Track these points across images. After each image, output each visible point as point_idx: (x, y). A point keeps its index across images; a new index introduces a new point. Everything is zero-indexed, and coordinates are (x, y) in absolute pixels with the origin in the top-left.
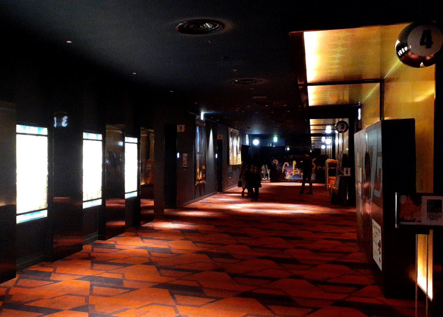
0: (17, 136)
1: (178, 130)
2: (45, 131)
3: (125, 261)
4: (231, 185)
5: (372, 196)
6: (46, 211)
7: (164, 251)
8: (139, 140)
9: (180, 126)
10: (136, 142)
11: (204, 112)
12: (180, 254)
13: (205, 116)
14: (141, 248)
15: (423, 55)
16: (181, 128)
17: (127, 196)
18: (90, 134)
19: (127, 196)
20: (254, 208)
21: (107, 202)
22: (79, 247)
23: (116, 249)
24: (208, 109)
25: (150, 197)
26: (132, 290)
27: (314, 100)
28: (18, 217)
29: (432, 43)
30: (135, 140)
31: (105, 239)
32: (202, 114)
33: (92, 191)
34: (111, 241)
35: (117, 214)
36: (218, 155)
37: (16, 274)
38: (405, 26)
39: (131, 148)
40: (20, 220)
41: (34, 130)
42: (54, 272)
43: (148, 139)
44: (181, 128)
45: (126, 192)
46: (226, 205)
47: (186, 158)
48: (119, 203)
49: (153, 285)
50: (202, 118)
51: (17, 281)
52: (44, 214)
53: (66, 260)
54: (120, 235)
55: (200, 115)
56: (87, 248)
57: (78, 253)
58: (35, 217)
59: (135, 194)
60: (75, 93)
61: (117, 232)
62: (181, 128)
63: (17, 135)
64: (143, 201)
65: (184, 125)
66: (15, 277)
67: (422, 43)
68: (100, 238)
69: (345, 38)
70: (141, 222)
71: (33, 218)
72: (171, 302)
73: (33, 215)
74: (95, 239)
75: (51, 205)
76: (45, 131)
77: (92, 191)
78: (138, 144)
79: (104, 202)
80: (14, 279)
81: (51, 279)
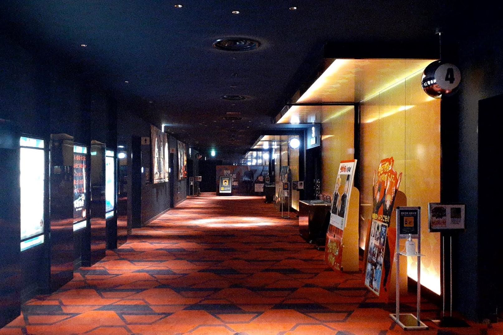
5: (440, 206)
7: (168, 272)
9: (144, 138)
10: (113, 155)
12: (186, 274)
14: (139, 271)
15: (444, 88)
21: (52, 223)
24: (167, 121)
26: (167, 314)
29: (454, 80)
34: (98, 266)
38: (428, 63)
44: (146, 140)
48: (60, 225)
49: (185, 307)
52: (41, 240)
54: (102, 260)
56: (77, 275)
57: (70, 283)
60: (86, 101)
61: (100, 256)
62: (146, 140)
63: (21, 149)
66: (19, 315)
67: (447, 79)
68: (84, 265)
69: (356, 67)
72: (217, 322)
74: (79, 266)
78: (46, 149)
79: (89, 224)
80: (19, 317)
81: (65, 311)
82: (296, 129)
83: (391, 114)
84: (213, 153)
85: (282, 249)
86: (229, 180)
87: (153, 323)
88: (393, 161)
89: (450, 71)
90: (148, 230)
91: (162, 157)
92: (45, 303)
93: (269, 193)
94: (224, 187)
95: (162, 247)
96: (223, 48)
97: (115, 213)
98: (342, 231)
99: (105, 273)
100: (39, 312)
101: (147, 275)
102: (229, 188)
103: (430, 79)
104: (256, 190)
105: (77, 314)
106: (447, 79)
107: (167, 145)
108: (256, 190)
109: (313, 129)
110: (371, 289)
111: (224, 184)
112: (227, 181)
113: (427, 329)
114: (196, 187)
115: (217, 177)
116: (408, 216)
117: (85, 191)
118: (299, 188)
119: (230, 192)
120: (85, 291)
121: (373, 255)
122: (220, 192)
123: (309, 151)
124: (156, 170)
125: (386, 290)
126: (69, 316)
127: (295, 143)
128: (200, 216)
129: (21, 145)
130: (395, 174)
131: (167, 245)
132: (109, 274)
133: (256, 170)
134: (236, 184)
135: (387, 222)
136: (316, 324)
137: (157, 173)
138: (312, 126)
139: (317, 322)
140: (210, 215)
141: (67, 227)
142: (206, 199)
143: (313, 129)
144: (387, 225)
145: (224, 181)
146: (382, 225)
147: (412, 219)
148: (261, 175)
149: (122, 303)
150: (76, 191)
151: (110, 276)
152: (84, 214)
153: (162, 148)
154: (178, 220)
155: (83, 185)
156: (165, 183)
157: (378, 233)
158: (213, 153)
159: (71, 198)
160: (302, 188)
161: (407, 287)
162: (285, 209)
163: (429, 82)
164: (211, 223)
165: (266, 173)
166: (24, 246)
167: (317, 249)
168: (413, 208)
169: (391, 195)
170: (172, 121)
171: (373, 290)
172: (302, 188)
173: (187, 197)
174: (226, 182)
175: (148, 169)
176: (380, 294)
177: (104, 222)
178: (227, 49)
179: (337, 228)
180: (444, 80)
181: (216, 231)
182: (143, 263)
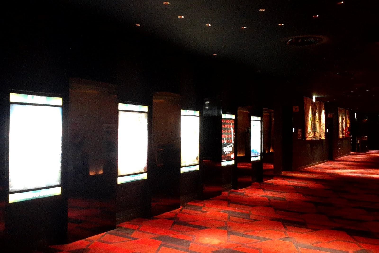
0: (182, 116)
1: (294, 110)
2: (198, 113)
3: (253, 203)
4: (341, 155)
6: (59, 189)
7: (284, 199)
8: (261, 119)
11: (315, 95)
13: (317, 99)
16: (295, 109)
17: (253, 159)
18: (226, 115)
19: (253, 159)
20: (357, 173)
21: (238, 164)
22: (220, 193)
23: (244, 195)
25: (271, 162)
27: (324, 136)
28: (119, 179)
30: (259, 118)
31: (237, 189)
32: (314, 98)
33: (190, 156)
35: (244, 172)
36: (328, 130)
37: (180, 206)
39: (256, 125)
40: (120, 181)
41: (191, 112)
42: (204, 206)
43: (270, 117)
45: (11, 189)
46: (335, 170)
47: (300, 132)
50: (314, 100)
51: (181, 210)
52: (144, 176)
53: (210, 200)
55: (312, 98)
58: (135, 179)
59: (259, 158)
62: (296, 109)
64: (264, 165)
65: (299, 129)
66: (179, 207)
70: (264, 179)
71: (133, 179)
73: (133, 177)
75: (150, 168)
76: (198, 113)
77: (190, 156)
78: (261, 121)
87: (244, 223)
91: (318, 120)
97: (261, 158)
99: (243, 194)
100: (190, 208)
107: (323, 111)
117: (233, 142)
124: (309, 130)
126: (202, 212)
128: (346, 166)
129: (182, 114)
131: (298, 183)
137: (310, 133)
140: (356, 167)
149: (244, 211)
150: (225, 141)
151: (244, 196)
152: (232, 156)
153: (317, 114)
154: (328, 168)
155: (231, 138)
156: (321, 141)
159: (220, 146)
164: (351, 173)
166: (183, 170)
173: (351, 153)
175: (300, 130)
177: (251, 164)
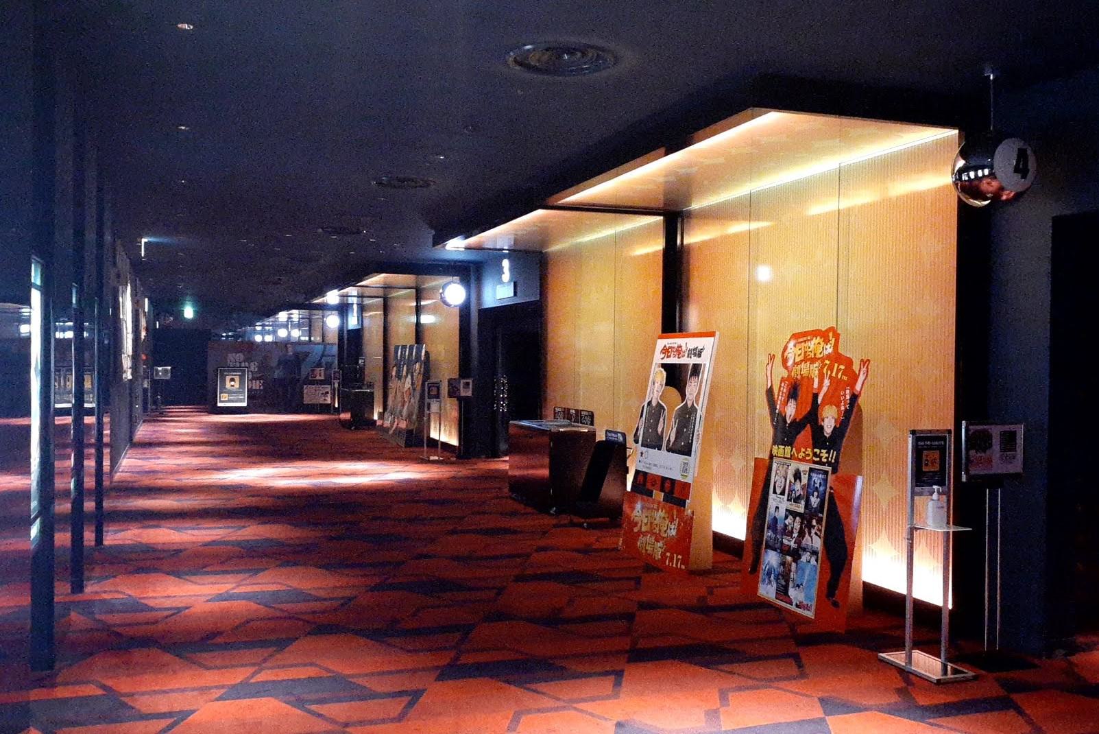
67: (1017, 170)
82: (455, 261)
83: (825, 234)
84: (189, 312)
85: (506, 531)
86: (242, 378)
88: (837, 336)
89: (1022, 155)
90: (128, 497)
92: (61, 692)
93: (358, 404)
94: (230, 392)
95: (214, 538)
96: (529, 68)
98: (686, 486)
101: (254, 606)
102: (241, 396)
103: (975, 169)
104: (307, 401)
105: (193, 712)
106: (1017, 170)
108: (307, 401)
109: (506, 264)
110: (788, 606)
111: (228, 385)
112: (237, 379)
113: (975, 678)
114: (155, 394)
115: (210, 369)
116: (930, 448)
118: (463, 394)
119: (245, 404)
120: (138, 655)
121: (787, 532)
122: (219, 405)
123: (485, 314)
125: (835, 604)
127: (455, 293)
130: (849, 362)
132: (152, 609)
133: (307, 354)
134: (257, 385)
135: (829, 464)
136: (757, 688)
138: (505, 256)
139: (750, 682)
141: (531, 472)
142: (185, 425)
143: (506, 264)
144: (829, 469)
145: (228, 378)
146: (811, 470)
147: (936, 454)
148: (319, 365)
154: (173, 472)
157: (798, 486)
158: (189, 312)
160: (469, 393)
161: (861, 595)
162: (414, 443)
163: (972, 174)
165: (329, 359)
167: (581, 525)
168: (930, 431)
169: (838, 406)
170: (154, 235)
171: (793, 608)
172: (469, 393)
174: (232, 380)
176: (816, 614)
178: (545, 71)
179: (664, 479)
180: (1011, 169)
181: (289, 496)
182: (212, 578)
